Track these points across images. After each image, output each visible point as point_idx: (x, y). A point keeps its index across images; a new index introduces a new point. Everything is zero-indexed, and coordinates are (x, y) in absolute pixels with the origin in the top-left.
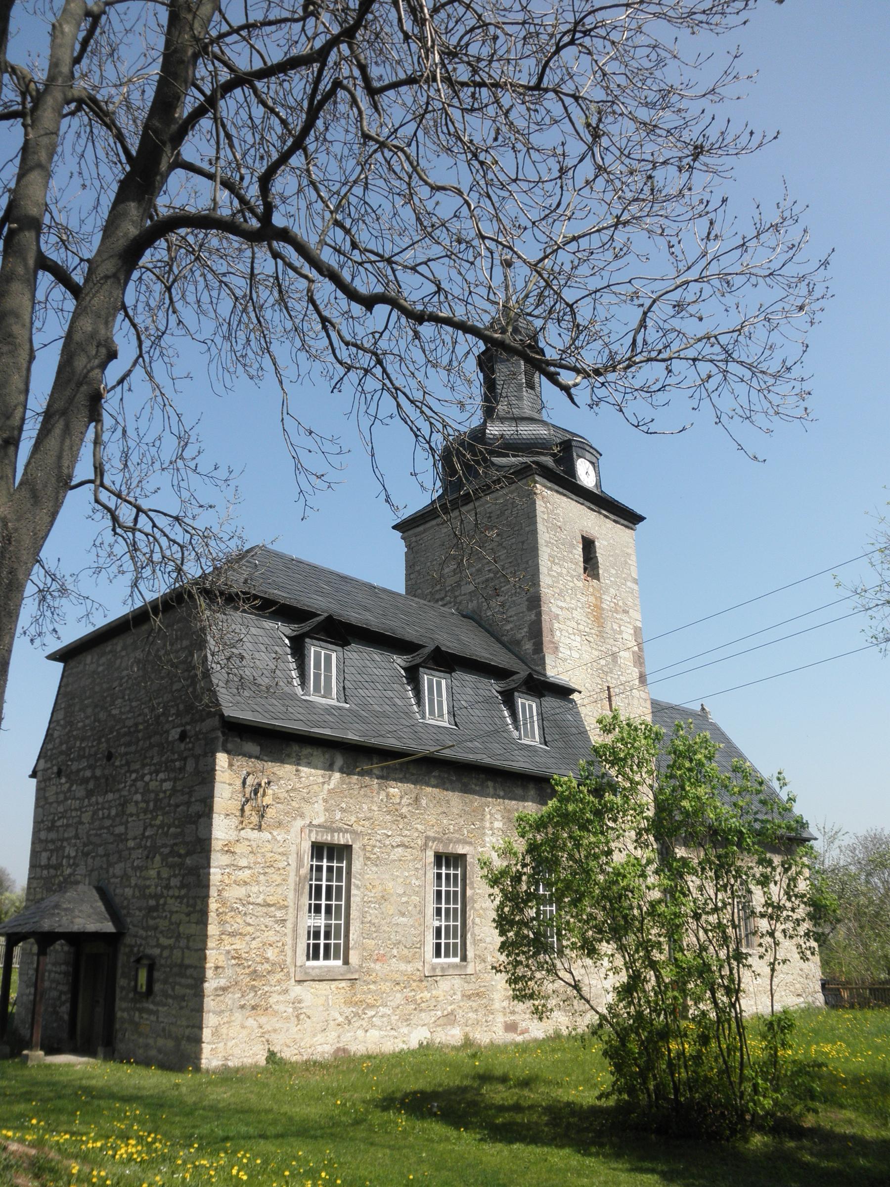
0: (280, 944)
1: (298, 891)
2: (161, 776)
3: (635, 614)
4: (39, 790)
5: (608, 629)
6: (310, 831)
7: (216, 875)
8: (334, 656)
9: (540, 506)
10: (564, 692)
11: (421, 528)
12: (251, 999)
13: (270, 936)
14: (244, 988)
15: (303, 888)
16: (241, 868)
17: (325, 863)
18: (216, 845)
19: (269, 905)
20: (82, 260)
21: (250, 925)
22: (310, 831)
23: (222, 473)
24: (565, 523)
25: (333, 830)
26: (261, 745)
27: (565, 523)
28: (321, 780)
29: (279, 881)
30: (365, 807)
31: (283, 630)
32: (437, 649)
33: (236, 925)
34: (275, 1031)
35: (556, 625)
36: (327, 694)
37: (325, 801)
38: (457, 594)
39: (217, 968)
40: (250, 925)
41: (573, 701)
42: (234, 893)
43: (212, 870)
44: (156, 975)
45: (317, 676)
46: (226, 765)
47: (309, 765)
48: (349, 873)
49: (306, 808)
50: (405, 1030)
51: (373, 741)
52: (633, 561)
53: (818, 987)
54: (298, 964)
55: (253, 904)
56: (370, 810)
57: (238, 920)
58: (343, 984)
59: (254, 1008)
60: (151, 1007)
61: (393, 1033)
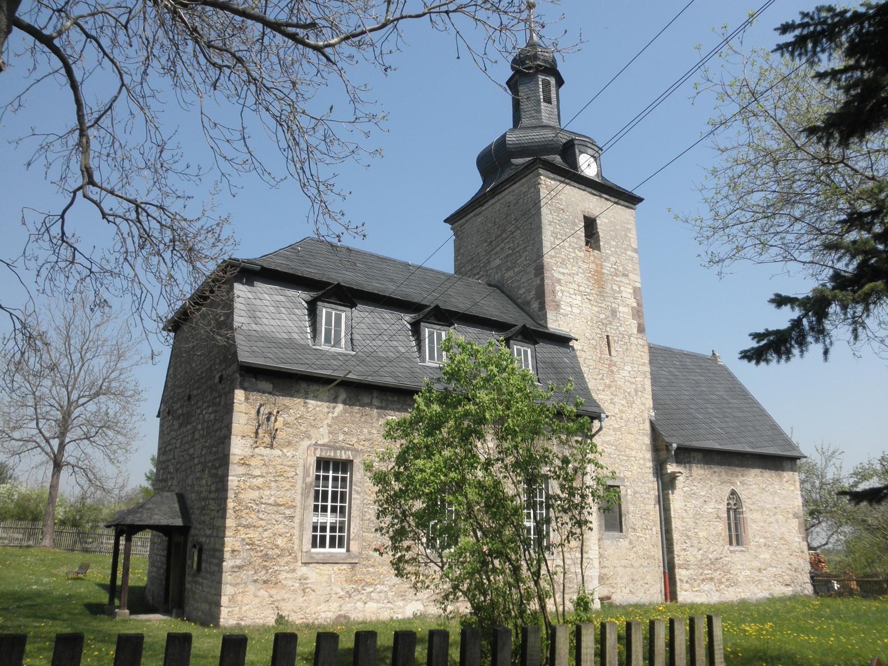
0: (288, 535)
1: (305, 495)
2: (210, 410)
3: (636, 279)
4: (161, 425)
5: (608, 290)
6: (315, 449)
7: (233, 481)
8: (343, 315)
9: (543, 192)
10: (563, 341)
11: (463, 220)
12: (262, 575)
13: (280, 528)
14: (257, 567)
15: (309, 493)
16: (255, 477)
17: (331, 474)
18: (234, 459)
19: (279, 505)
20: (54, 11)
21: (262, 519)
22: (315, 449)
23: (193, 170)
24: (567, 206)
25: (335, 449)
26: (272, 383)
27: (567, 206)
28: (326, 410)
29: (288, 486)
30: (366, 431)
31: (300, 297)
32: (437, 307)
33: (250, 520)
34: (283, 600)
35: (558, 288)
36: (337, 343)
37: (329, 426)
38: (487, 268)
39: (233, 551)
40: (262, 519)
41: (572, 347)
42: (249, 495)
43: (230, 478)
44: (204, 557)
45: (328, 332)
46: (243, 399)
47: (315, 398)
48: (351, 482)
49: (313, 432)
50: (401, 604)
51: (370, 379)
52: (633, 234)
53: (807, 579)
54: (305, 550)
55: (265, 504)
56: (370, 433)
57: (252, 516)
58: (345, 566)
59: (265, 582)
60: (200, 580)
61: (389, 605)
